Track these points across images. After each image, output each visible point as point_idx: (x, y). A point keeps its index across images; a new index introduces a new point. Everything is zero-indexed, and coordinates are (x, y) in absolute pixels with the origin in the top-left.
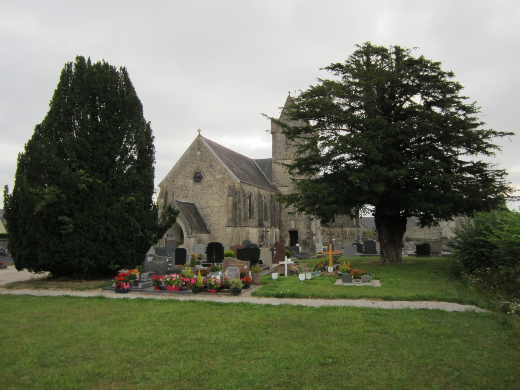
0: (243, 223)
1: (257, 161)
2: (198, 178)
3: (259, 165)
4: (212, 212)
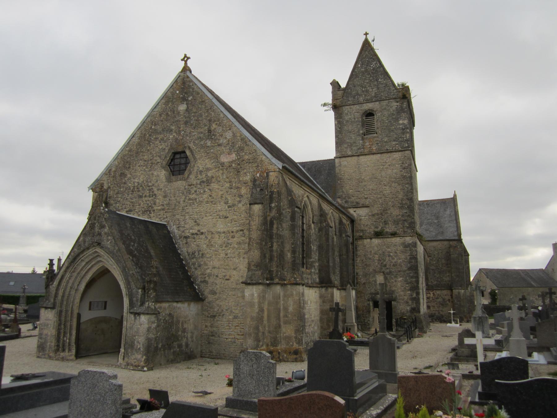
0: (288, 275)
1: (304, 164)
2: (178, 163)
3: (309, 170)
4: (210, 245)
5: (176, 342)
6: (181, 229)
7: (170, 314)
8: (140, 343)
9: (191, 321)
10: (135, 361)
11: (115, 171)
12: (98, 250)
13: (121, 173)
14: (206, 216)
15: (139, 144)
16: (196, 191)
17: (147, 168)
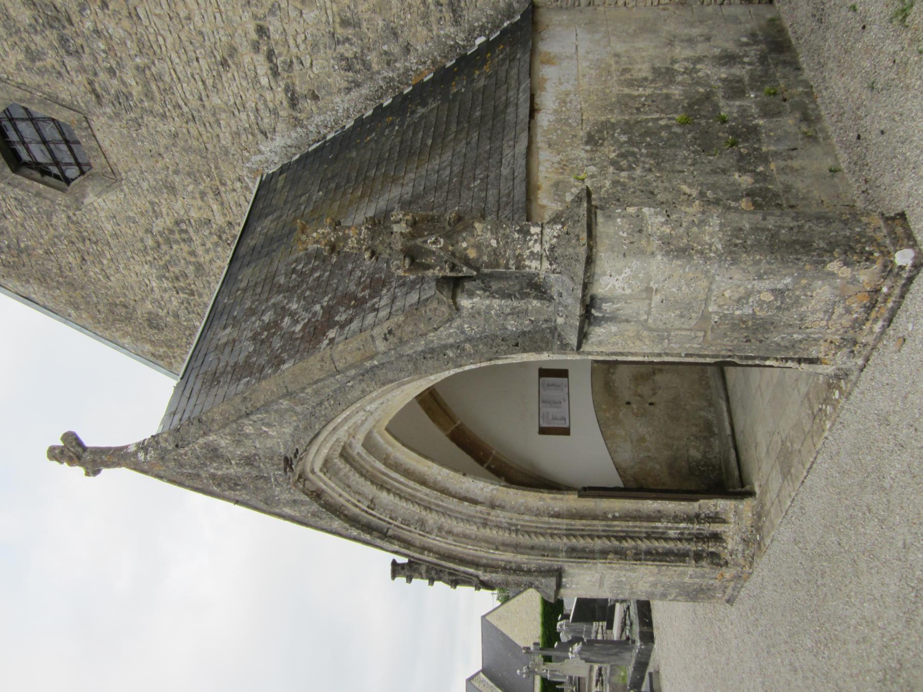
5: (716, 108)
6: (267, 121)
7: (590, 139)
8: (749, 294)
9: (620, 48)
10: (839, 310)
11: (152, 343)
12: (315, 459)
13: (151, 326)
14: (189, 18)
15: (43, 279)
16: (111, 71)
17: (101, 254)
